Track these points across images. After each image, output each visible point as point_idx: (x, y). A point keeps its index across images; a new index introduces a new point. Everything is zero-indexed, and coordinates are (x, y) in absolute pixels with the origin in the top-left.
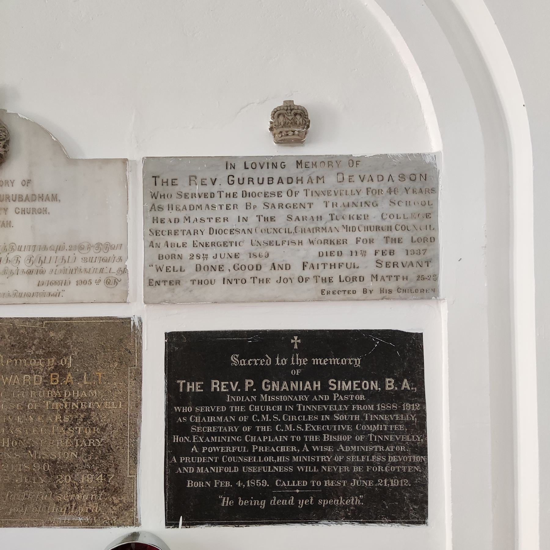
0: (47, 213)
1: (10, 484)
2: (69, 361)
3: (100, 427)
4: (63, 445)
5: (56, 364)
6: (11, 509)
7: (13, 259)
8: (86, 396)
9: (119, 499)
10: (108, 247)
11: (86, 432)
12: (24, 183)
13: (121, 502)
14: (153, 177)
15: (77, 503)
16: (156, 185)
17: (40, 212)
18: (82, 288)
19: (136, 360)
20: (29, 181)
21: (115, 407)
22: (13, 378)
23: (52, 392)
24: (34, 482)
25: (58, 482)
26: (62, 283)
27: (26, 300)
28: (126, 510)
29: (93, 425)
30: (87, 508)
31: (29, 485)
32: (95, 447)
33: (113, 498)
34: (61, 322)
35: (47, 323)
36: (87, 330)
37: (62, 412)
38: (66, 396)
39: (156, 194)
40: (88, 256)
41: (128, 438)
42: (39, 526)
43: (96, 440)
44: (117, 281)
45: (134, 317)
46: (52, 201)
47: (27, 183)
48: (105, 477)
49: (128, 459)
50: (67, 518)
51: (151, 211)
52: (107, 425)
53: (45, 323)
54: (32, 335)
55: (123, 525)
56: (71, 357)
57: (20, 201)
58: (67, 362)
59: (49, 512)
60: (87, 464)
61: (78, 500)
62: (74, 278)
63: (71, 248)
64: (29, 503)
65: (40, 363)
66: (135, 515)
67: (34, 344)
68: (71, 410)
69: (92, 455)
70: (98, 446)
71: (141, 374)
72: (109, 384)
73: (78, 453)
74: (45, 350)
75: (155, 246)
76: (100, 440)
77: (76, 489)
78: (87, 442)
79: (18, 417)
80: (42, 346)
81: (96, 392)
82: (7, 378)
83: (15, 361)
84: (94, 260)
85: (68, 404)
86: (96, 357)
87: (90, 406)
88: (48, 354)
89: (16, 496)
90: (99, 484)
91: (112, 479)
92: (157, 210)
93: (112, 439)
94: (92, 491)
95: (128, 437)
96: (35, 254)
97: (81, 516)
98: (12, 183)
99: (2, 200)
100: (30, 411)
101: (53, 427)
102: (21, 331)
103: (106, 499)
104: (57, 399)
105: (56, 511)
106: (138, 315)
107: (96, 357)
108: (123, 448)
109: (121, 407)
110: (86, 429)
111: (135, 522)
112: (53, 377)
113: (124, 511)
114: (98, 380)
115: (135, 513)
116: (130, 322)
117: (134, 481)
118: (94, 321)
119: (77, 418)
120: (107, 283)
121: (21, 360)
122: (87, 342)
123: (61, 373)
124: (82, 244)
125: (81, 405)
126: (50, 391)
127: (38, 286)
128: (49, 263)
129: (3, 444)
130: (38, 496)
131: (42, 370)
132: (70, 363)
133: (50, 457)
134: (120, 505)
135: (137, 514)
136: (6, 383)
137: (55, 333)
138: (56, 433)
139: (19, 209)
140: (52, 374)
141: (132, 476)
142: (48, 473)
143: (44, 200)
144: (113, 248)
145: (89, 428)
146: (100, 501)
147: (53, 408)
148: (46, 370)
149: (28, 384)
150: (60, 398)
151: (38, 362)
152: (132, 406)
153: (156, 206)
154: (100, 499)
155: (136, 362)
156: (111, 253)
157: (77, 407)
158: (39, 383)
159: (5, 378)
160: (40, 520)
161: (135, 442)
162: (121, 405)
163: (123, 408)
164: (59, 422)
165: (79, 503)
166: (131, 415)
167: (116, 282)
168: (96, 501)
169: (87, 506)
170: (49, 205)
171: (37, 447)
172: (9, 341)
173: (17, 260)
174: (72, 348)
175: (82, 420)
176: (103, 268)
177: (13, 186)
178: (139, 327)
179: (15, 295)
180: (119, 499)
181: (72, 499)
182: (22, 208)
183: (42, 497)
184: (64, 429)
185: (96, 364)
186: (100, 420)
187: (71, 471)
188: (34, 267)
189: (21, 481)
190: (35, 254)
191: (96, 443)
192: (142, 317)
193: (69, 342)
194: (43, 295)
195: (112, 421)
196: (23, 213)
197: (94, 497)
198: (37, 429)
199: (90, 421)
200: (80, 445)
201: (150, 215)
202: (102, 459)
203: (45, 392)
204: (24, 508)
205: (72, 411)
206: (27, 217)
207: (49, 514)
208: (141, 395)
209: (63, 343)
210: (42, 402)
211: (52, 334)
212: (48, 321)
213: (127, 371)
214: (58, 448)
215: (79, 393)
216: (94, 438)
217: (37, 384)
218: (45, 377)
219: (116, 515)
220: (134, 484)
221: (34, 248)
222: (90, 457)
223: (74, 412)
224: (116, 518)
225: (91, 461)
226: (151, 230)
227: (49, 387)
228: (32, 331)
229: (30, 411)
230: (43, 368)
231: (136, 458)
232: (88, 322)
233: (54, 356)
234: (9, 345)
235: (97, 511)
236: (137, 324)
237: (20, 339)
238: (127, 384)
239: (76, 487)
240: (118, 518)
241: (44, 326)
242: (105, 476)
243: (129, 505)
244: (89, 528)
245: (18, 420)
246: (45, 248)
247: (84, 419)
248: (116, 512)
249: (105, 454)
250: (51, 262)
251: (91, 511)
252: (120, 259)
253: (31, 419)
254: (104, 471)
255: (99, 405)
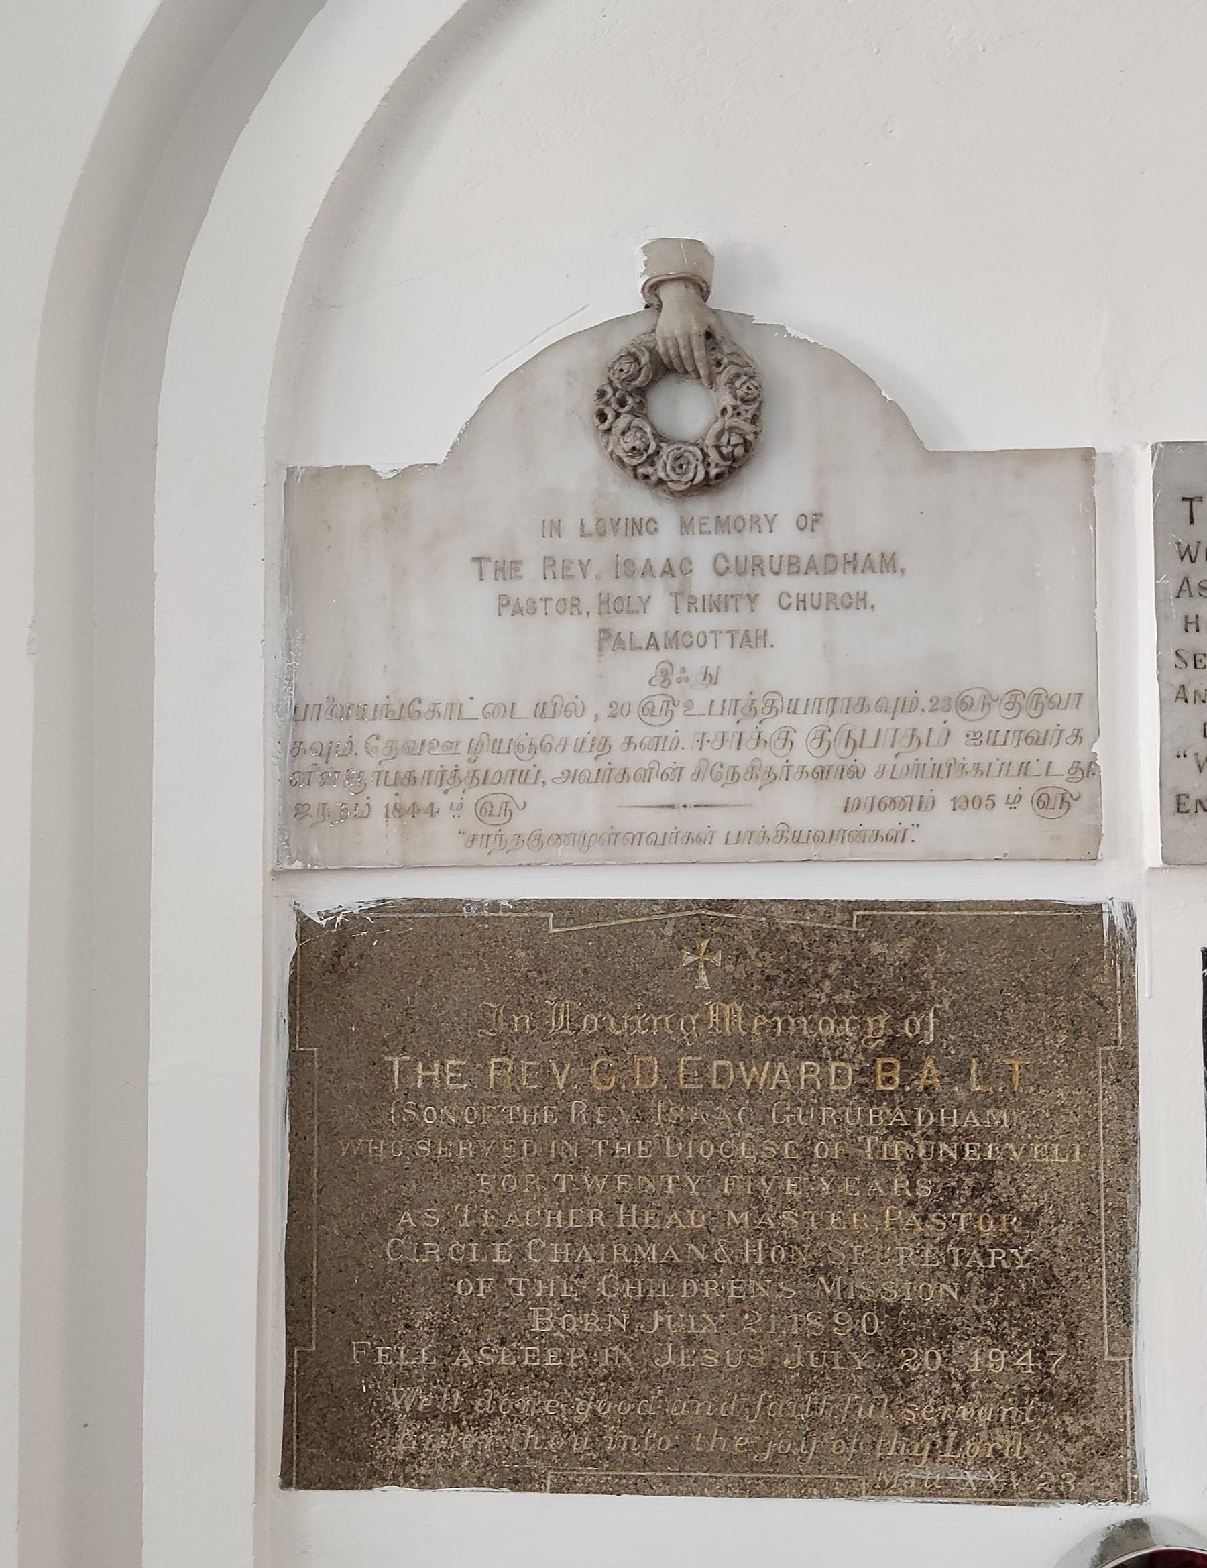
0: (869, 606)
1: (769, 1371)
2: (928, 1023)
3: (1018, 1214)
4: (916, 1262)
5: (891, 1033)
6: (770, 1444)
7: (776, 736)
8: (978, 1125)
9: (1083, 1423)
10: (1041, 701)
11: (981, 1229)
12: (802, 522)
13: (1088, 1430)
14: (1184, 499)
15: (962, 1431)
16: (1192, 522)
17: (847, 604)
18: (968, 817)
19: (1120, 1026)
20: (818, 517)
21: (1063, 1161)
22: (772, 1071)
23: (881, 1113)
24: (837, 1367)
25: (906, 1368)
26: (911, 805)
27: (812, 850)
28: (1102, 1454)
29: (999, 1208)
30: (991, 1446)
31: (823, 1375)
32: (1009, 1271)
33: (1066, 1419)
34: (903, 913)
35: (863, 916)
36: (979, 937)
37: (913, 1168)
38: (920, 1124)
39: (1193, 550)
40: (984, 726)
41: (1103, 1250)
42: (853, 1495)
43: (1012, 1251)
44: (1067, 797)
45: (1110, 902)
46: (882, 572)
47: (811, 522)
48: (1040, 1358)
49: (1105, 1308)
50: (933, 1473)
51: (1178, 597)
52: (1041, 1207)
53: (858, 916)
54: (822, 950)
55: (1097, 1497)
56: (932, 1015)
57: (793, 573)
58: (922, 1029)
59: (879, 1454)
60: (986, 1319)
61: (962, 1421)
62: (945, 791)
63: (937, 705)
64: (824, 1426)
65: (847, 1029)
66: (1129, 1470)
67: (827, 976)
68: (937, 1163)
69: (1001, 1292)
70: (1017, 1268)
71: (1135, 1066)
72: (1041, 1092)
73: (961, 1287)
74: (858, 991)
75: (1190, 697)
76: (1021, 1252)
77: (957, 1390)
78: (986, 1256)
79: (789, 1181)
80: (852, 981)
81: (1005, 1115)
82: (754, 1069)
83: (776, 1022)
84: (1001, 739)
85: (928, 1147)
86: (1003, 1015)
87: (990, 1153)
88: (870, 1005)
89: (785, 1406)
90: (1023, 1379)
91: (1060, 1367)
92: (1195, 593)
93: (1055, 1250)
94: (1003, 1398)
95: (1103, 1247)
96: (835, 724)
97: (972, 1469)
98: (771, 523)
99: (742, 571)
100: (821, 1164)
101: (888, 1212)
102: (792, 938)
103: (1045, 1421)
104: (896, 1131)
105: (902, 1452)
106: (1122, 896)
107: (1003, 1015)
108: (1089, 1277)
109: (1078, 1159)
110: (981, 1220)
111: (1129, 1491)
112: (883, 1070)
113: (1096, 1458)
114: (1011, 1080)
115: (1129, 1464)
116: (1100, 916)
117: (1123, 1371)
118: (997, 914)
119: (953, 1188)
120: (1041, 804)
121: (792, 1021)
122: (978, 972)
123: (905, 1058)
124: (968, 693)
125: (963, 1150)
126: (875, 1108)
127: (845, 811)
128: (875, 746)
129: (747, 1256)
130: (847, 1408)
131: (852, 1049)
132: (931, 1029)
133: (880, 1297)
134: (1086, 1439)
135: (1134, 1467)
136: (752, 1084)
137: (886, 945)
138: (897, 1227)
139: (789, 596)
140: (880, 1061)
141: (1118, 1359)
142: (874, 1341)
143: (859, 569)
144: (1055, 703)
145: (989, 1216)
146: (1027, 1426)
147: (885, 1157)
148: (865, 1050)
149: (814, 1086)
150: (906, 1128)
151: (841, 1027)
152: (1113, 1159)
153: (1194, 582)
154: (1027, 1419)
155: (1120, 1032)
156: (1049, 720)
157: (955, 1156)
158: (844, 1085)
159: (748, 1070)
160: (856, 1477)
161: (1123, 1261)
162: (1077, 1153)
163: (1084, 1164)
164: (903, 1197)
165: (967, 1431)
166: (1108, 1185)
167: (1066, 802)
168: (1017, 1427)
169: (989, 1439)
170: (871, 583)
171: (842, 1266)
172: (760, 965)
173: (786, 739)
174: (936, 987)
175: (968, 1193)
176: (1029, 763)
177: (771, 531)
178: (1125, 930)
179: (781, 837)
180: (1083, 1423)
181: (947, 1419)
182: (798, 594)
183: (861, 1409)
184: (917, 1218)
185: (1005, 1034)
186: (1020, 1196)
187: (941, 1338)
188: (832, 759)
189: (799, 1363)
190: (835, 724)
191: (1012, 1259)
192: (1133, 902)
193: (927, 971)
194: (859, 836)
195: (1054, 1198)
196: (801, 607)
197: (1009, 1413)
198: (840, 1214)
199: (991, 1198)
200: (965, 1263)
201: (1177, 610)
202: (1029, 1306)
203: (862, 1111)
204: (808, 1443)
205: (940, 1168)
206: (813, 618)
207: (881, 1460)
208: (1135, 1126)
209: (909, 973)
210: (854, 1140)
211: (877, 948)
212: (866, 910)
213: (1093, 1057)
214: (904, 1270)
215: (958, 1117)
216: (1006, 1245)
217: (840, 1088)
218: (862, 1069)
219: (1075, 1469)
220: (1124, 1383)
221: (831, 703)
222: (994, 1298)
223: (945, 1169)
224: (1074, 1478)
225: (999, 1310)
226: (1180, 653)
227: (873, 1096)
228: (820, 939)
229: (821, 1164)
230: (856, 1042)
231: (1126, 1305)
232: (978, 916)
233: (886, 1008)
234: (759, 977)
235: (1021, 1455)
236: (1120, 922)
237: (788, 960)
238: (1095, 1096)
239: (955, 1385)
240: (1080, 1477)
241: (854, 925)
242: (1041, 1356)
243: (1111, 1441)
244: (997, 1503)
245: (788, 1189)
246: (863, 705)
247: (974, 1189)
248: (1073, 1460)
249: (1038, 1293)
250: (880, 743)
251: (1002, 1455)
252: (1078, 736)
253: (826, 1186)
254: (1037, 1342)
255: (1017, 1150)
